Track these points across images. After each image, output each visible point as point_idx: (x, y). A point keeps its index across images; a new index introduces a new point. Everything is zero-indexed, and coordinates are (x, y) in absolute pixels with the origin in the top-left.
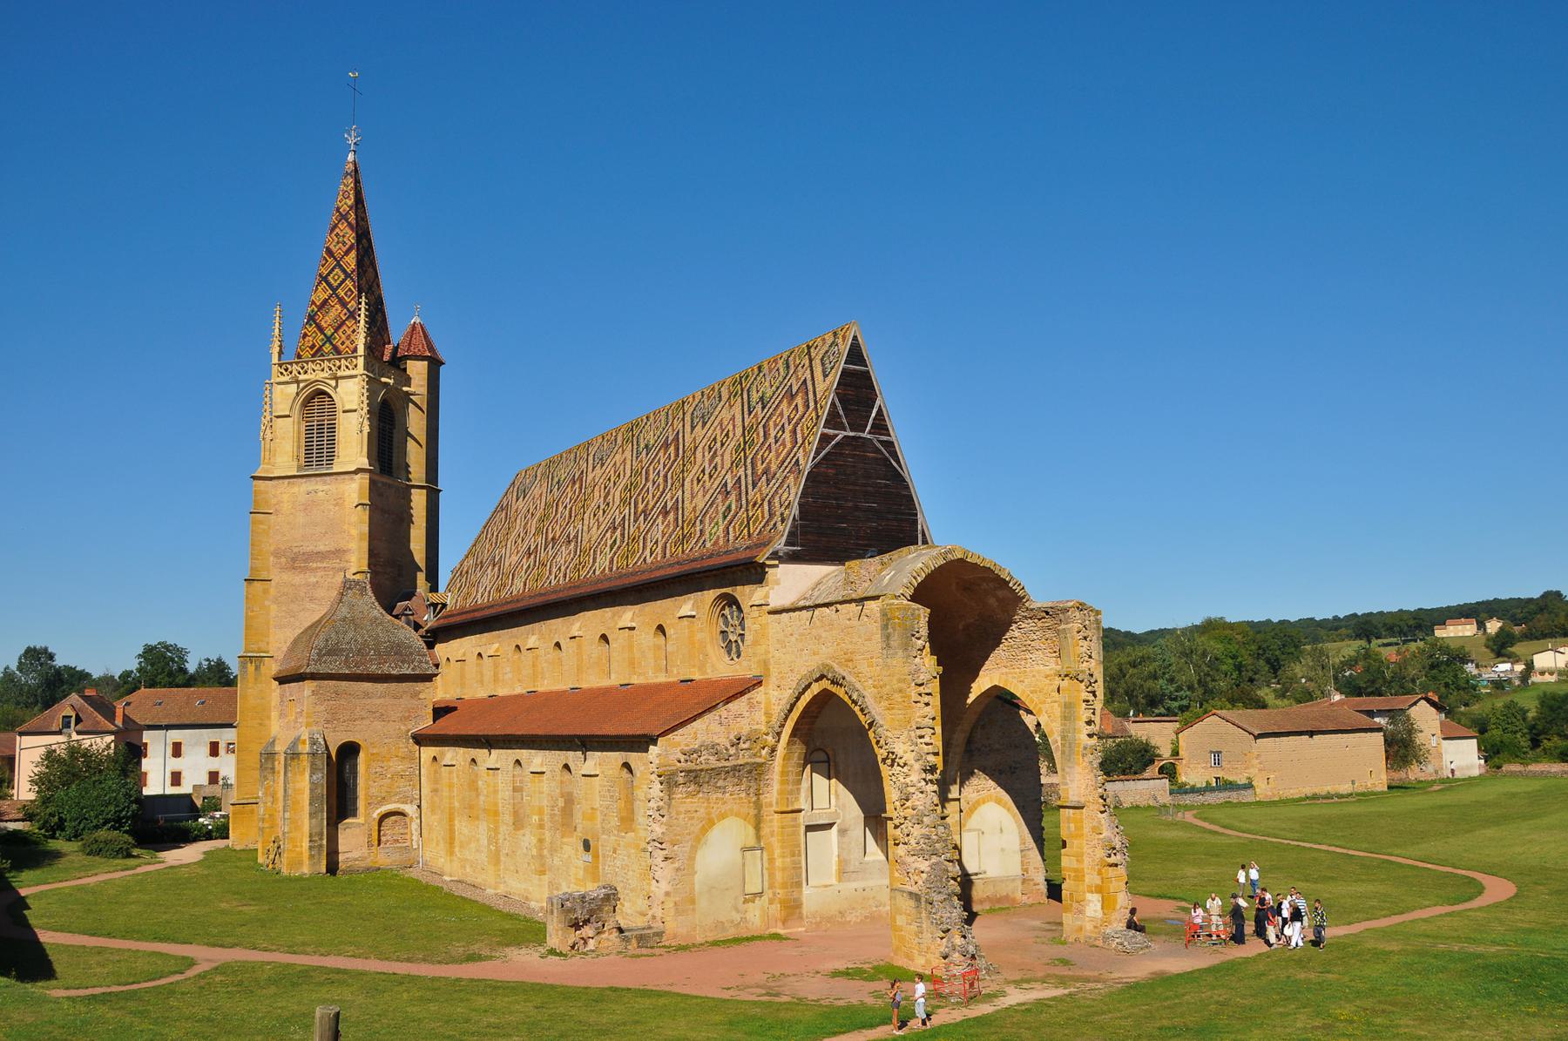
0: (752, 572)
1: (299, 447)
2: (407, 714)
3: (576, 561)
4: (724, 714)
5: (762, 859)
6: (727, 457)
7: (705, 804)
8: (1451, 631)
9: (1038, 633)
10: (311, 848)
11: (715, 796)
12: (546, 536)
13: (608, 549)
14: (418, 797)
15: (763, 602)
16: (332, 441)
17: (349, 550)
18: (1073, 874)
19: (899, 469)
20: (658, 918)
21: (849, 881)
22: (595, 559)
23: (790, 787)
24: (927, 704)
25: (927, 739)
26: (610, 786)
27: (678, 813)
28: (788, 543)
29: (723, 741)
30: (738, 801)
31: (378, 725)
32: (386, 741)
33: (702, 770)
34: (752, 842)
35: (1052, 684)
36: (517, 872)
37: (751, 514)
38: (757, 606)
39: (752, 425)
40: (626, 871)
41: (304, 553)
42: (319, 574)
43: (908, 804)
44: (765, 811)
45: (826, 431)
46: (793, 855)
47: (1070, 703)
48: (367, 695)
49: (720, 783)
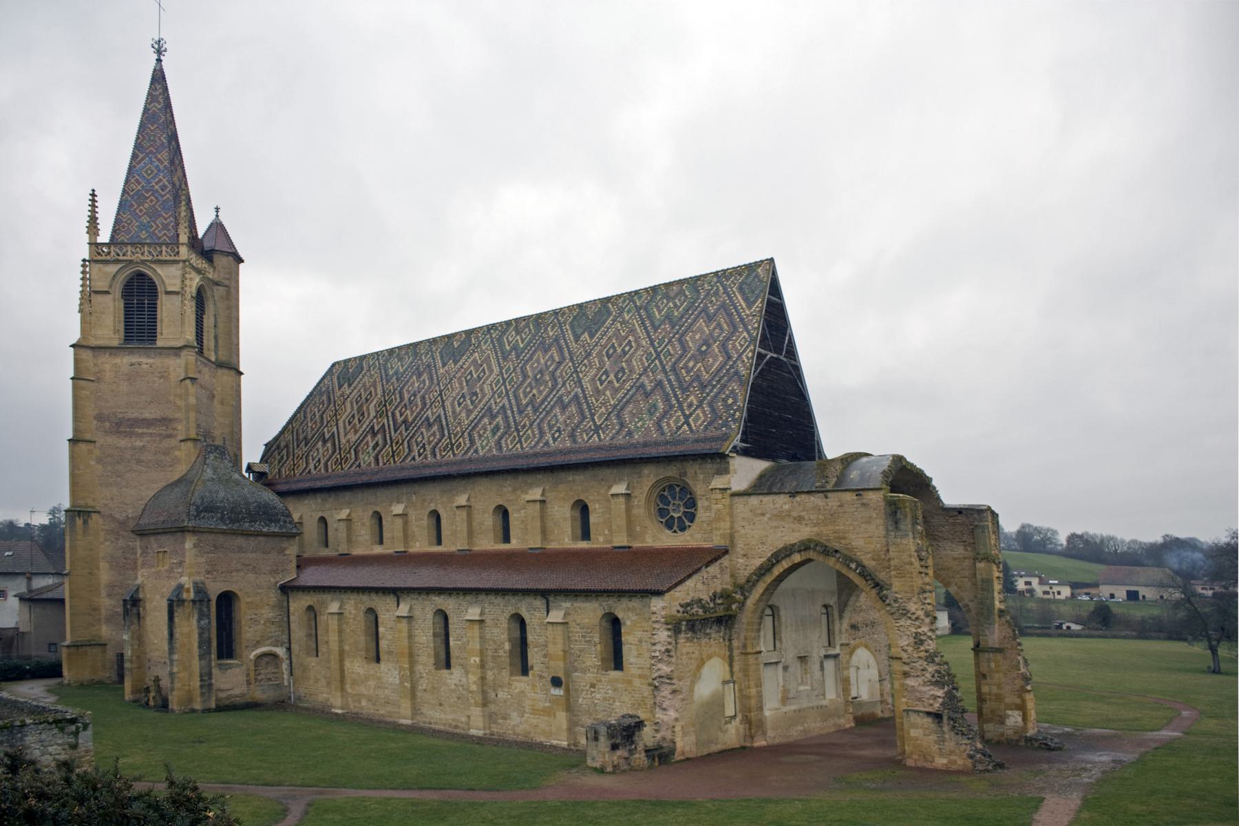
0: (716, 459)
1: (119, 322)
2: (275, 568)
3: (445, 441)
10: (201, 686)
14: (287, 641)
15: (726, 486)
17: (175, 420)
20: (668, 740)
21: (790, 705)
22: (472, 442)
25: (928, 601)
27: (682, 654)
28: (742, 441)
29: (705, 597)
31: (251, 576)
32: (259, 591)
33: (697, 620)
34: (728, 677)
36: (441, 705)
38: (720, 489)
39: (664, 337)
41: (129, 420)
42: (146, 439)
43: (922, 648)
44: (736, 652)
45: (761, 350)
46: (757, 687)
48: (241, 549)
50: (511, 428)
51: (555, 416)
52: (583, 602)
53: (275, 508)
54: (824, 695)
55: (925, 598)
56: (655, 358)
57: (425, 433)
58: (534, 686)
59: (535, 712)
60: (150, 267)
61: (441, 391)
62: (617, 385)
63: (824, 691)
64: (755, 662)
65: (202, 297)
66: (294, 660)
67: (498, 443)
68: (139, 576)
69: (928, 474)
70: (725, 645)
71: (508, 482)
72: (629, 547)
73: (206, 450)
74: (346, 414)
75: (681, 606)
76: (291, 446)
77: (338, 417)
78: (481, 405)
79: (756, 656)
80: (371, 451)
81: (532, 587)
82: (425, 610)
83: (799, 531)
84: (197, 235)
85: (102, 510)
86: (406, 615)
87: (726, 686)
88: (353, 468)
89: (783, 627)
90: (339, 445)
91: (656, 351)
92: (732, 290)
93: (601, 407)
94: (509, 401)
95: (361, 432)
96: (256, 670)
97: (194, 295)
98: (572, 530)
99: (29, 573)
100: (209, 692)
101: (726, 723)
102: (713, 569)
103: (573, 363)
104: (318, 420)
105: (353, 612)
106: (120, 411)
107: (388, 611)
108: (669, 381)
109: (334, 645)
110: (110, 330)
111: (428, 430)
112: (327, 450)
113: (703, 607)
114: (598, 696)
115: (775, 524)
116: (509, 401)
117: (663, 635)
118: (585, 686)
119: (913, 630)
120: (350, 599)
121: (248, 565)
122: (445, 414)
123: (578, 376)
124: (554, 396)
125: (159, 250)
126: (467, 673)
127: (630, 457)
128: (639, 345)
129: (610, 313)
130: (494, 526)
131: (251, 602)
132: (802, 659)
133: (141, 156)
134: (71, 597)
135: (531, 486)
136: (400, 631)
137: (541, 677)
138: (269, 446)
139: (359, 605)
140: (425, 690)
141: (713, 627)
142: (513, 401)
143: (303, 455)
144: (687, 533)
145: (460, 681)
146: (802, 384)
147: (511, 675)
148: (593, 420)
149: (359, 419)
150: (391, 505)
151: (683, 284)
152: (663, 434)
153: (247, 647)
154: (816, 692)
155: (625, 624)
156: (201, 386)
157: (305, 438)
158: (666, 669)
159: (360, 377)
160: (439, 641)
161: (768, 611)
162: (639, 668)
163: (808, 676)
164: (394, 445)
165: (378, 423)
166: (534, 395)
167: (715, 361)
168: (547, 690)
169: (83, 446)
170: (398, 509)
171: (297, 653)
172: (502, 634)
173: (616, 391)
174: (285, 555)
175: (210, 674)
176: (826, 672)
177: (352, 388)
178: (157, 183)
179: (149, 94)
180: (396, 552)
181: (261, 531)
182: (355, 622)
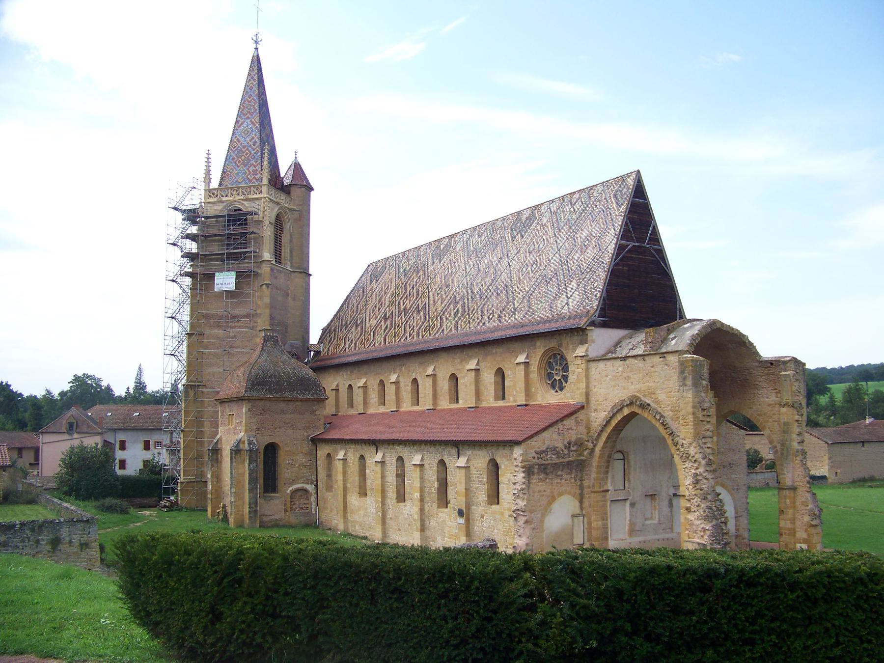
0: (577, 333)
2: (308, 425)
4: (561, 427)
5: (583, 522)
6: (387, 300)
7: (550, 487)
9: (764, 377)
10: (250, 512)
11: (556, 481)
12: (399, 308)
13: (452, 317)
14: (315, 480)
18: (787, 532)
19: (665, 268)
22: (442, 324)
23: (602, 475)
24: (708, 422)
25: (709, 445)
26: (479, 474)
27: (534, 492)
29: (560, 445)
30: (570, 485)
31: (290, 432)
32: (295, 442)
33: (548, 464)
35: (772, 410)
36: (399, 530)
37: (396, 330)
44: (586, 491)
46: (603, 520)
47: (788, 423)
48: (283, 412)
49: (559, 473)
52: (478, 450)
54: (671, 529)
55: (705, 443)
57: (415, 318)
58: (450, 516)
61: (429, 284)
62: (531, 275)
63: (672, 525)
64: (603, 499)
71: (458, 355)
72: (526, 405)
73: (265, 339)
74: (372, 304)
78: (451, 295)
79: (604, 493)
80: (453, 318)
83: (628, 389)
84: (279, 174)
87: (576, 519)
88: (370, 347)
89: (632, 469)
95: (378, 318)
96: (291, 502)
97: (273, 222)
98: (495, 392)
100: (255, 516)
102: (568, 423)
104: (355, 310)
105: (352, 458)
107: (371, 457)
109: (340, 483)
111: (417, 315)
112: (358, 333)
115: (613, 383)
117: (520, 476)
118: (478, 517)
119: (693, 471)
120: (350, 448)
121: (288, 423)
122: (429, 303)
127: (527, 333)
130: (450, 390)
131: (290, 451)
132: (652, 496)
133: (241, 121)
135: (471, 357)
136: (376, 473)
140: (391, 518)
141: (564, 470)
146: (666, 264)
148: (514, 304)
150: (390, 375)
153: (285, 484)
154: (663, 526)
158: (522, 504)
159: (384, 274)
162: (508, 503)
165: (390, 311)
168: (457, 519)
170: (393, 378)
172: (434, 475)
175: (256, 503)
178: (250, 141)
180: (392, 411)
181: (297, 398)
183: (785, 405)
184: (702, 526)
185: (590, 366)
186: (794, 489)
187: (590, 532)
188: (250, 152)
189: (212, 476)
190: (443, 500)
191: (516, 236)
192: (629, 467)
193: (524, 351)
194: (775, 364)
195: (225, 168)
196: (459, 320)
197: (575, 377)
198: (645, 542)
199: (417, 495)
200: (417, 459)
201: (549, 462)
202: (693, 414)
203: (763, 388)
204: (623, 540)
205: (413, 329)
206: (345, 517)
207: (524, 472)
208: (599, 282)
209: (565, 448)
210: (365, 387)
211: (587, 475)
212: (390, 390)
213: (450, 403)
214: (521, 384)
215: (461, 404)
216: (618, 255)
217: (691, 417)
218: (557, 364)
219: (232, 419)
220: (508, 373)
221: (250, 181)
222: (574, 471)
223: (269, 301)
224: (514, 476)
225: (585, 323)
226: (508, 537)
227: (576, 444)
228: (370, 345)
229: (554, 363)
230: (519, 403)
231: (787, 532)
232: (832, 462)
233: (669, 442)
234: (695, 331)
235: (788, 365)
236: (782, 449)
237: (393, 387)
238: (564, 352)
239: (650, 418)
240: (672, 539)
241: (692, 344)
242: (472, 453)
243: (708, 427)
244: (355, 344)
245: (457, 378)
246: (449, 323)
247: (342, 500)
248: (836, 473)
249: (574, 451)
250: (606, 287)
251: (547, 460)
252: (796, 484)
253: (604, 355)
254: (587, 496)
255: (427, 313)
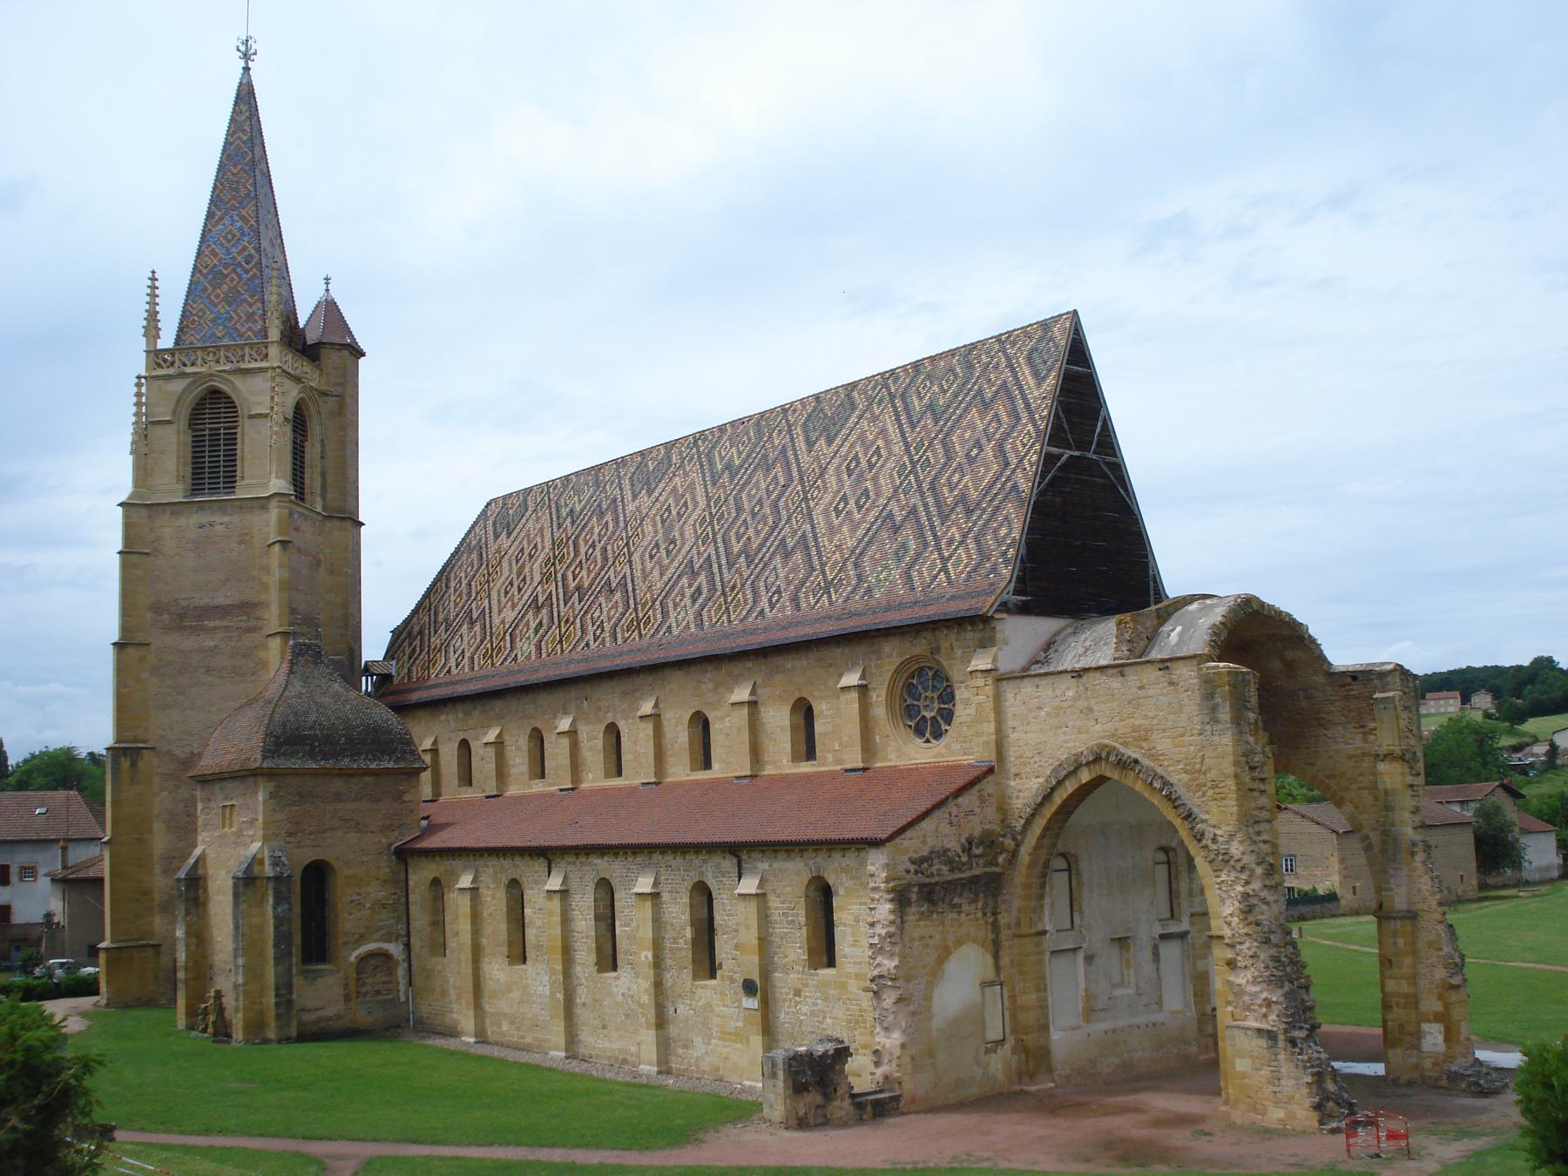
2: (388, 823)
3: (630, 615)
8: (1432, 707)
10: (277, 1004)
13: (687, 600)
14: (404, 933)
16: (231, 458)
22: (665, 615)
23: (1034, 903)
25: (1265, 837)
27: (912, 940)
28: (1016, 592)
29: (953, 845)
31: (352, 837)
36: (604, 1027)
37: (563, 630)
38: (982, 671)
40: (821, 1019)
41: (195, 608)
44: (1005, 934)
46: (1039, 990)
48: (338, 797)
49: (956, 900)
50: (716, 590)
51: (775, 568)
53: (390, 733)
54: (1159, 1003)
55: (1258, 833)
56: (910, 472)
57: (604, 605)
58: (722, 994)
59: (725, 1036)
60: (228, 380)
61: (628, 538)
62: (857, 516)
65: (303, 416)
66: (414, 963)
67: (699, 614)
68: (199, 843)
69: (1299, 618)
70: (986, 923)
71: (708, 675)
73: (293, 652)
74: (502, 579)
75: (913, 862)
76: (427, 632)
77: (492, 585)
78: (680, 558)
79: (1036, 939)
80: (532, 636)
81: (718, 840)
82: (583, 879)
83: (1087, 732)
84: (297, 322)
85: (157, 745)
86: (558, 888)
88: (506, 663)
90: (491, 628)
91: (911, 461)
92: (1018, 362)
93: (834, 552)
94: (716, 549)
95: (520, 607)
96: (358, 979)
97: (290, 416)
99: (64, 839)
101: (988, 1051)
103: (803, 486)
104: (465, 591)
106: (183, 596)
107: (536, 882)
108: (926, 505)
109: (466, 937)
110: (171, 487)
111: (608, 599)
113: (950, 862)
114: (805, 1009)
116: (716, 549)
117: (885, 909)
118: (788, 994)
119: (1239, 888)
122: (632, 574)
123: (808, 507)
124: (776, 538)
125: (240, 353)
126: (637, 975)
128: (890, 453)
129: (853, 407)
130: (691, 743)
132: (1122, 942)
134: (112, 876)
135: (736, 680)
137: (732, 980)
138: (397, 632)
139: (499, 875)
140: (584, 1005)
141: (965, 895)
142: (722, 549)
143: (442, 644)
144: (944, 740)
145: (629, 989)
146: (1126, 490)
147: (695, 977)
148: (824, 573)
149: (519, 587)
151: (953, 355)
152: (913, 589)
153: (346, 944)
155: (837, 894)
156: (299, 550)
157: (446, 620)
158: (889, 964)
160: (603, 927)
161: (1060, 863)
162: (855, 963)
163: (1132, 971)
164: (563, 624)
166: (749, 539)
167: (988, 469)
168: (740, 1001)
169: (131, 651)
171: (418, 951)
173: (854, 527)
174: (404, 802)
175: (289, 986)
176: (1162, 964)
177: (512, 538)
178: (239, 253)
179: (232, 120)
180: (561, 790)
182: (495, 902)
183: (1385, 756)
184: (1265, 995)
185: (1003, 689)
186: (1412, 916)
187: (1014, 1017)
188: (240, 277)
189: (188, 933)
190: (706, 962)
191: (815, 442)
192: (1080, 884)
193: (855, 664)
194: (1364, 679)
195: (188, 307)
196: (703, 607)
197: (971, 711)
198: (1114, 1031)
199: (647, 955)
200: (644, 884)
201: (937, 879)
202: (1236, 776)
203: (1335, 724)
204: (1074, 1029)
205: (601, 626)
206: (478, 1006)
207: (891, 900)
208: (1012, 525)
209: (963, 852)
210: (499, 744)
211: (1004, 902)
212: (557, 752)
213: (692, 770)
214: (853, 729)
215: (718, 770)
216: (1043, 478)
217: (1231, 783)
218: (926, 689)
219: (231, 815)
220: (821, 708)
221: (241, 336)
222: (981, 895)
223: (287, 575)
224: (871, 909)
225: (991, 607)
226: (856, 1033)
227: (981, 843)
228: (505, 659)
229: (919, 687)
230: (848, 766)
231: (1402, 1001)
232: (1345, 868)
233: (1184, 833)
234: (1217, 615)
235: (1389, 678)
236: (1384, 842)
237: (565, 742)
238: (945, 663)
239: (1139, 787)
240: (1163, 1024)
241: (1214, 641)
242: (770, 866)
243: (1263, 801)
244: (472, 659)
245: (619, 732)
246: (683, 613)
247: (470, 971)
248: (1354, 888)
249: (979, 856)
250: (1024, 536)
251: (932, 875)
252: (1415, 908)
253: (1025, 669)
254: (1007, 944)
255: (631, 594)
